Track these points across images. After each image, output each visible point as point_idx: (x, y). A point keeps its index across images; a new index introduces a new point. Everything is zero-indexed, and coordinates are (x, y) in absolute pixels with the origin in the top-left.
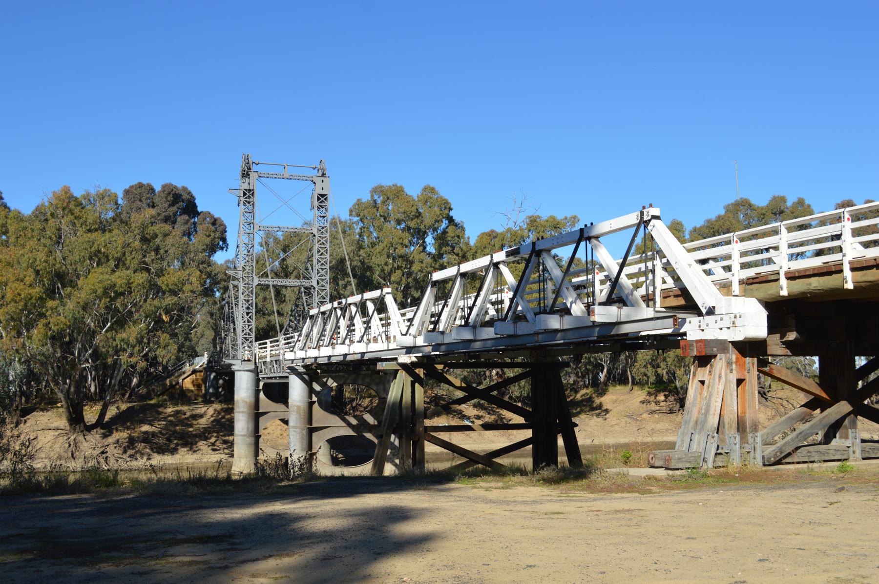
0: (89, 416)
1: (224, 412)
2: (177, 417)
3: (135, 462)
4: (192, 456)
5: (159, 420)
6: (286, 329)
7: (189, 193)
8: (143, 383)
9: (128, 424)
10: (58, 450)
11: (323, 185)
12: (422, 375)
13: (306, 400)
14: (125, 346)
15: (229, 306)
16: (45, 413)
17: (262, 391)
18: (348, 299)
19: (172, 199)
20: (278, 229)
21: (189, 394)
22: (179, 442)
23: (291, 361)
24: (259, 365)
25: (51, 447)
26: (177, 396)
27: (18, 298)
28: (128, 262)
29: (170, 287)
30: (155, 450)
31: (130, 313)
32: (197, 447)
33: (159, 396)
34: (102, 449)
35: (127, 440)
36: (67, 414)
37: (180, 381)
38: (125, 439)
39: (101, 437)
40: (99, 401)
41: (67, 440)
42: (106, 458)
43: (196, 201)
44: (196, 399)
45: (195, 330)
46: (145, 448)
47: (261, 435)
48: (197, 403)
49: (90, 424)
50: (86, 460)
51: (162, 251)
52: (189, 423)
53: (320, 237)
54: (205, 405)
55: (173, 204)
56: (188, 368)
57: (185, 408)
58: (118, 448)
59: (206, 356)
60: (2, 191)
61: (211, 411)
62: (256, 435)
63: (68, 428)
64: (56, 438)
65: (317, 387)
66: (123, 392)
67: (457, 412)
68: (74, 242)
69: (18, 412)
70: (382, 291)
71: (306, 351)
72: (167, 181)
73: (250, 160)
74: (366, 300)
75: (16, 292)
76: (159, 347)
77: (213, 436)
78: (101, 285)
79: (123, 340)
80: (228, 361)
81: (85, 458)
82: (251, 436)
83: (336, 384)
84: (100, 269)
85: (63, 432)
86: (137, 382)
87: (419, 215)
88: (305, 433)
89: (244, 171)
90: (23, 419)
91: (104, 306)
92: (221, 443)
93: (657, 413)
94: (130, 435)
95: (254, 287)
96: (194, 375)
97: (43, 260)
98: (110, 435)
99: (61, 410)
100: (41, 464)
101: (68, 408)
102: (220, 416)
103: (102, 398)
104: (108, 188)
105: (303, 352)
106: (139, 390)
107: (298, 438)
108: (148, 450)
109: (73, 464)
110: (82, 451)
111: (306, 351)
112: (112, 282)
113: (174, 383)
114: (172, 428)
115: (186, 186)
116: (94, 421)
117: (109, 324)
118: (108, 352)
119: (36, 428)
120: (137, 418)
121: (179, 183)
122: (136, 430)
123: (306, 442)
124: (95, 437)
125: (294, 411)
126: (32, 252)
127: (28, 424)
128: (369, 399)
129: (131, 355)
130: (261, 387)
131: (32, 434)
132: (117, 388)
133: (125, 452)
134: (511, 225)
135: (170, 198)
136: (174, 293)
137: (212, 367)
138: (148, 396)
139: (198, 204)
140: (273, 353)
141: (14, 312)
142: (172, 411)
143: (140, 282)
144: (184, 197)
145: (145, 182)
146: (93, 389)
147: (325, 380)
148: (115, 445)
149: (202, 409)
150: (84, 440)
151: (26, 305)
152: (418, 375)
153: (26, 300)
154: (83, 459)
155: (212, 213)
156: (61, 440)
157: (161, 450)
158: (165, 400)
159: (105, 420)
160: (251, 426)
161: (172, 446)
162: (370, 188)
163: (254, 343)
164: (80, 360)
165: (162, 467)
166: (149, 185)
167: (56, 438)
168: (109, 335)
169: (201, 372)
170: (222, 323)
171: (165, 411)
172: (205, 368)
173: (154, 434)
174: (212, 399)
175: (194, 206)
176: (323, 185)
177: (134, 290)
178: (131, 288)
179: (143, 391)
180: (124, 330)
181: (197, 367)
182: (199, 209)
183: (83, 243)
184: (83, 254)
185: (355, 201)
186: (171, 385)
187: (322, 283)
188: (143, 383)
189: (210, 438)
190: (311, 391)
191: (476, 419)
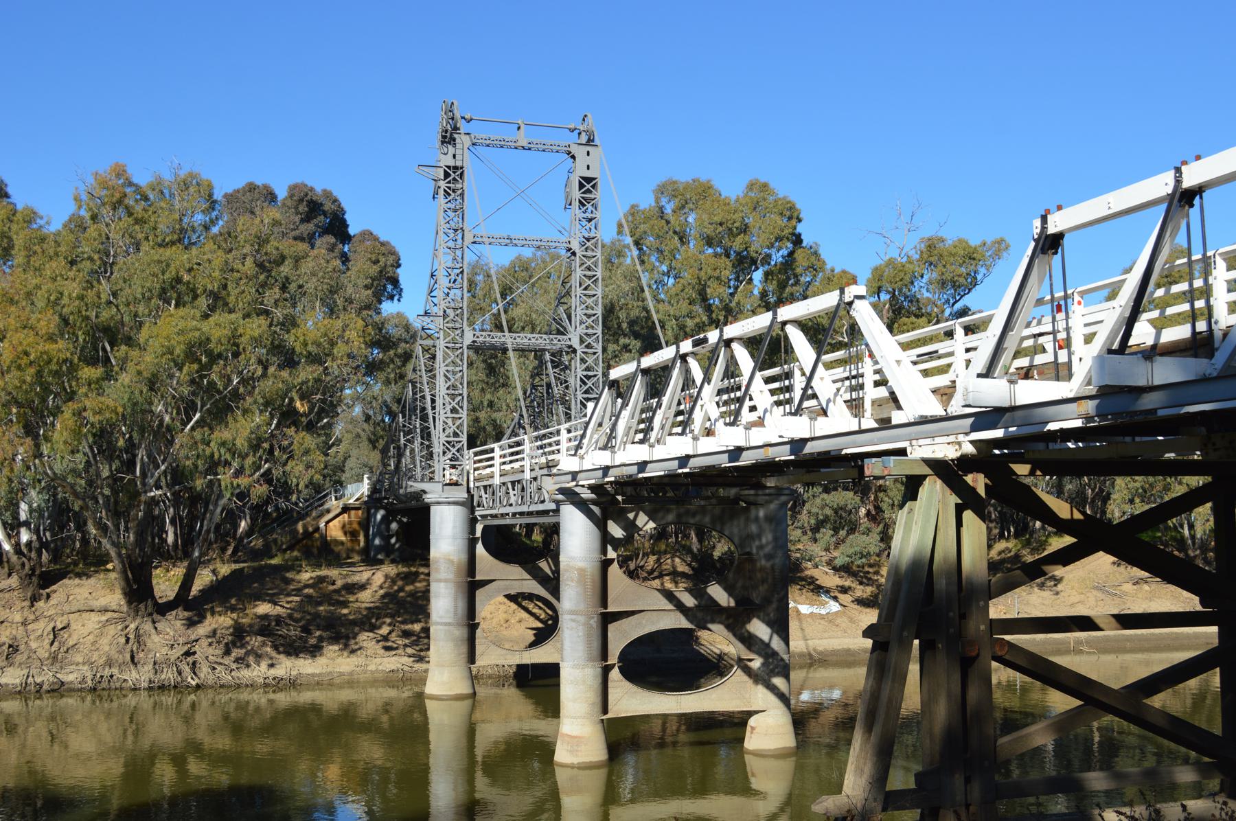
0: (163, 587)
1: (402, 579)
2: (320, 589)
3: (246, 671)
4: (348, 660)
5: (288, 595)
7: (335, 201)
8: (257, 529)
9: (233, 601)
10: (107, 648)
11: (588, 160)
12: (981, 491)
13: (597, 556)
14: (228, 456)
15: (414, 387)
16: (84, 581)
20: (509, 241)
21: (337, 549)
22: (324, 634)
23: (569, 477)
24: (475, 493)
25: (93, 644)
26: (315, 551)
27: (25, 361)
28: (232, 299)
29: (310, 348)
30: (281, 649)
31: (236, 395)
32: (356, 643)
33: (285, 551)
34: (186, 648)
35: (231, 630)
36: (123, 583)
37: (322, 525)
38: (228, 628)
39: (184, 625)
40: (181, 560)
41: (122, 630)
42: (194, 663)
43: (346, 217)
44: (349, 558)
45: (334, 450)
46: (264, 644)
47: (479, 624)
48: (352, 564)
49: (164, 600)
50: (157, 667)
51: (293, 287)
52: (341, 599)
54: (369, 568)
55: (307, 219)
56: (333, 504)
57: (333, 573)
58: (215, 645)
59: (366, 481)
60: (7, 180)
61: (379, 578)
62: (471, 624)
63: (125, 609)
64: (104, 626)
65: (616, 531)
66: (223, 544)
67: (806, 581)
68: (133, 264)
69: (35, 579)
70: (842, 292)
71: (652, 446)
72: (292, 181)
73: (455, 111)
74: (784, 323)
75: (20, 349)
77: (384, 623)
78: (181, 338)
79: (223, 444)
81: (155, 663)
82: (458, 624)
83: (654, 525)
84: (182, 311)
85: (116, 615)
86: (247, 528)
87: (745, 229)
88: (595, 625)
89: (446, 131)
90: (44, 592)
91: (188, 378)
92: (399, 636)
93: (1146, 582)
94: (236, 622)
95: (465, 347)
97: (74, 295)
98: (200, 622)
99: (113, 575)
100: (75, 675)
101: (124, 572)
102: (396, 588)
103: (187, 554)
104: (196, 170)
105: (608, 453)
106: (251, 542)
108: (268, 649)
109: (134, 674)
110: (150, 651)
112: (203, 333)
113: (311, 529)
114: (310, 609)
115: (328, 189)
116: (171, 595)
117: (198, 415)
118: (196, 467)
119: (66, 608)
120: (248, 591)
121: (319, 184)
122: (247, 612)
123: (596, 644)
124: (172, 625)
126: (54, 279)
127: (53, 601)
128: (655, 557)
129: (239, 473)
130: (478, 534)
131: (60, 619)
132: (212, 536)
133: (227, 652)
134: (893, 253)
135: (303, 208)
136: (315, 359)
137: (380, 500)
138: (266, 552)
141: (17, 387)
142: (311, 578)
143: (256, 335)
144: (326, 208)
145: (259, 182)
146: (170, 539)
147: (631, 516)
148: (210, 640)
149: (362, 574)
150: (153, 631)
151: (39, 374)
152: (974, 490)
153: (40, 366)
154: (151, 666)
156: (112, 630)
157: (293, 649)
158: (297, 559)
159: (192, 594)
160: (462, 605)
161: (313, 641)
162: (654, 186)
163: (466, 451)
164: (144, 484)
165: (294, 681)
166: (266, 187)
167: (104, 626)
168: (198, 435)
169: (357, 509)
170: (401, 420)
171: (298, 577)
172: (365, 502)
173: (279, 620)
174: (380, 557)
175: (344, 225)
176: (588, 160)
177: (244, 349)
178: (238, 346)
179: (257, 543)
180: (227, 426)
181: (351, 501)
182: (352, 231)
183: (149, 265)
184: (148, 285)
185: (627, 208)
186: (306, 533)
187: (589, 341)
188: (257, 529)
189: (380, 627)
190: (606, 539)
191: (841, 592)
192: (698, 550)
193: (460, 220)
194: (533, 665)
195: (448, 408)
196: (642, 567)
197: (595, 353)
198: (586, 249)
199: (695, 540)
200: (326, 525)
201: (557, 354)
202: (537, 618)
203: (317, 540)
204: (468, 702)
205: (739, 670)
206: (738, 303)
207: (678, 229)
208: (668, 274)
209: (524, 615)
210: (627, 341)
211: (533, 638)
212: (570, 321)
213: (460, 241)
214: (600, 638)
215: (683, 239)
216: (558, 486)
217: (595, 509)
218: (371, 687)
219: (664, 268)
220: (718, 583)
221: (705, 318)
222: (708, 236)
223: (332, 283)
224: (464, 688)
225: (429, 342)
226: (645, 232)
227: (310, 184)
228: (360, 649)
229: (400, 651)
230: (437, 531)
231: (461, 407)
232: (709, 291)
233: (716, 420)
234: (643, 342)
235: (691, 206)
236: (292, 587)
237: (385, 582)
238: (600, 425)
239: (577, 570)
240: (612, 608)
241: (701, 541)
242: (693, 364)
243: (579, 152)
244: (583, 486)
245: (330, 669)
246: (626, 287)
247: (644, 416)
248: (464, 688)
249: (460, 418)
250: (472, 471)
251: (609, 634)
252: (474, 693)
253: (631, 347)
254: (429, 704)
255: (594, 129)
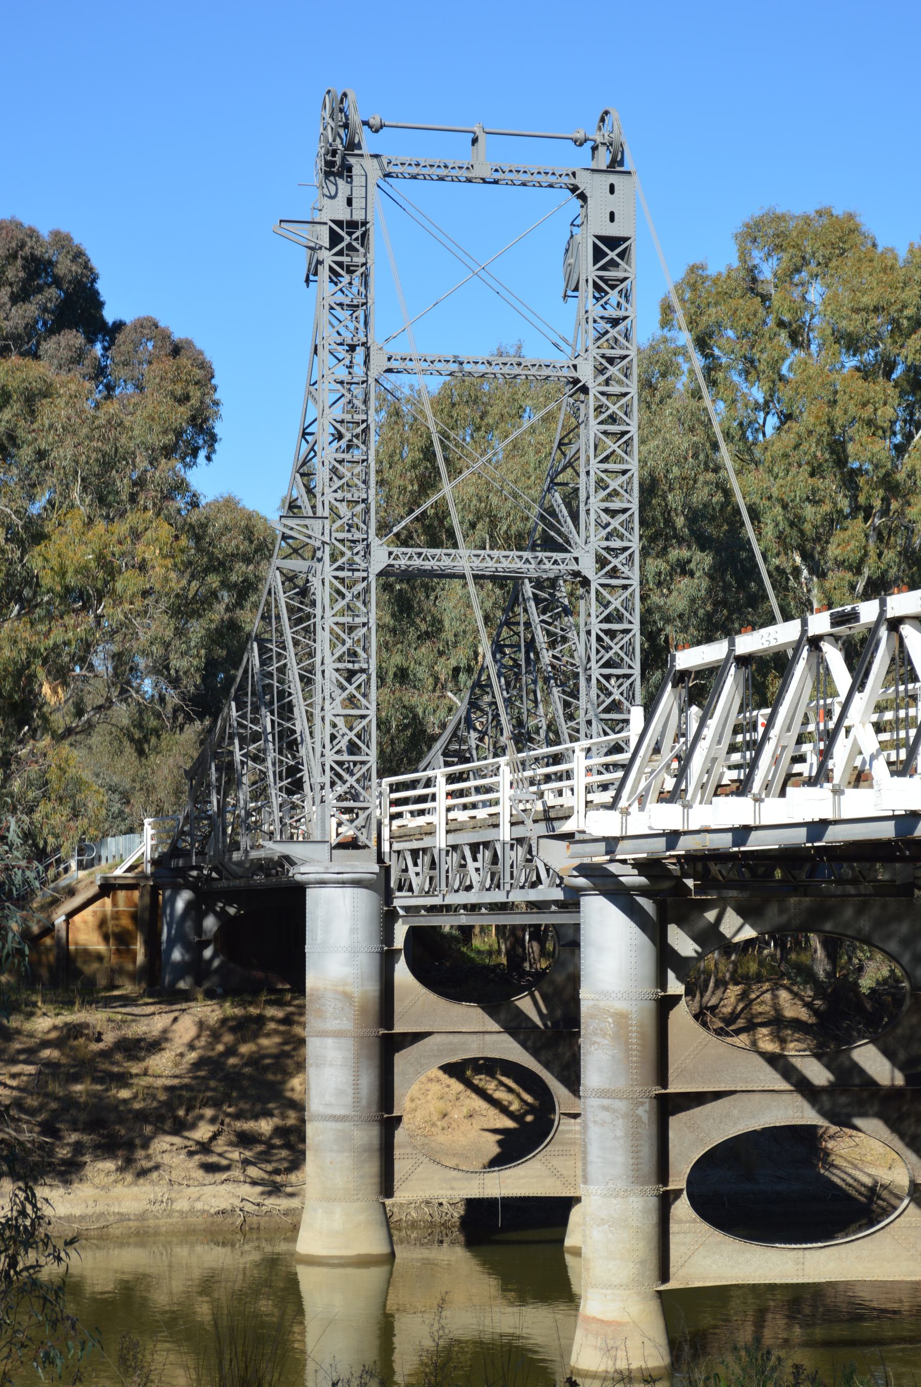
1: (233, 1030)
2: (72, 1048)
4: (135, 1189)
5: (13, 1061)
6: (454, 734)
7: (78, 255)
13: (649, 990)
15: (263, 650)
17: (403, 958)
18: (890, 600)
19: (22, 274)
22: (86, 1138)
37: (59, 920)
43: (100, 286)
47: (399, 1119)
52: (116, 1069)
53: (603, 394)
57: (96, 1017)
59: (148, 831)
71: (758, 800)
76: (46, 796)
77: (201, 1117)
80: (274, 849)
82: (369, 1121)
88: (645, 1117)
89: (334, 153)
92: (231, 1144)
95: (372, 578)
96: (108, 901)
102: (220, 1048)
105: (675, 809)
107: (620, 1133)
111: (626, 812)
113: (35, 929)
114: (54, 1087)
123: (648, 1151)
125: (604, 1036)
130: (399, 942)
137: (182, 872)
139: (104, 296)
140: (462, 816)
142: (55, 1028)
144: (61, 270)
147: (711, 916)
155: (162, 324)
160: (368, 1081)
161: (63, 1153)
170: (234, 713)
171: (28, 1026)
174: (182, 985)
181: (119, 872)
182: (110, 315)
185: (680, 273)
189: (193, 1126)
192: (828, 974)
193: (361, 326)
194: (505, 1200)
195: (340, 696)
196: (713, 1009)
197: (625, 587)
198: (607, 382)
199: (820, 953)
200: (67, 921)
201: (544, 584)
202: (504, 1109)
203: (48, 950)
204: (376, 1274)
205: (912, 1206)
206: (911, 474)
207: (786, 318)
208: (766, 407)
209: (479, 1103)
210: (685, 553)
211: (496, 1150)
212: (575, 517)
213: (359, 370)
214: (654, 1141)
215: (797, 339)
216: (576, 862)
217: (646, 903)
218: (181, 1243)
219: (758, 394)
220: (873, 1041)
221: (844, 504)
222: (850, 335)
223: (106, 448)
224: (376, 1246)
225: (296, 565)
226: (719, 325)
227: (27, 222)
228: (157, 1167)
229: (236, 1173)
230: (320, 937)
231: (365, 695)
232: (851, 448)
233: (873, 757)
234: (718, 552)
235: (813, 266)
236: (18, 1046)
237: (198, 1037)
238: (657, 750)
239: (613, 1015)
240: (675, 1087)
241: (832, 956)
242: (834, 656)
243: (596, 187)
244: (624, 862)
245: (100, 1208)
246: (683, 443)
247: (740, 738)
248: (376, 1246)
249: (363, 717)
250: (386, 821)
251: (671, 1135)
252: (393, 1255)
253: (692, 566)
254: (307, 1278)
255: (623, 139)
